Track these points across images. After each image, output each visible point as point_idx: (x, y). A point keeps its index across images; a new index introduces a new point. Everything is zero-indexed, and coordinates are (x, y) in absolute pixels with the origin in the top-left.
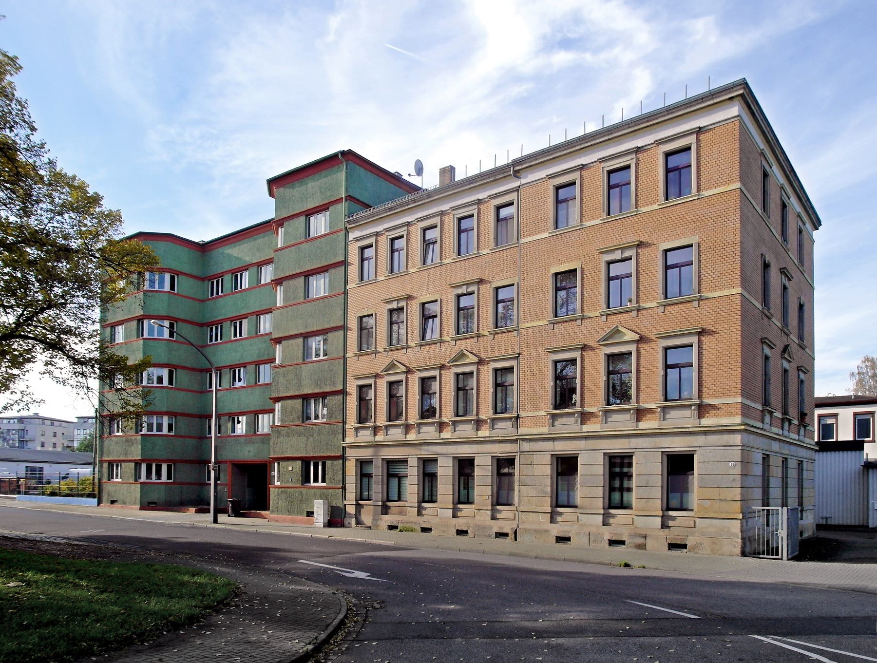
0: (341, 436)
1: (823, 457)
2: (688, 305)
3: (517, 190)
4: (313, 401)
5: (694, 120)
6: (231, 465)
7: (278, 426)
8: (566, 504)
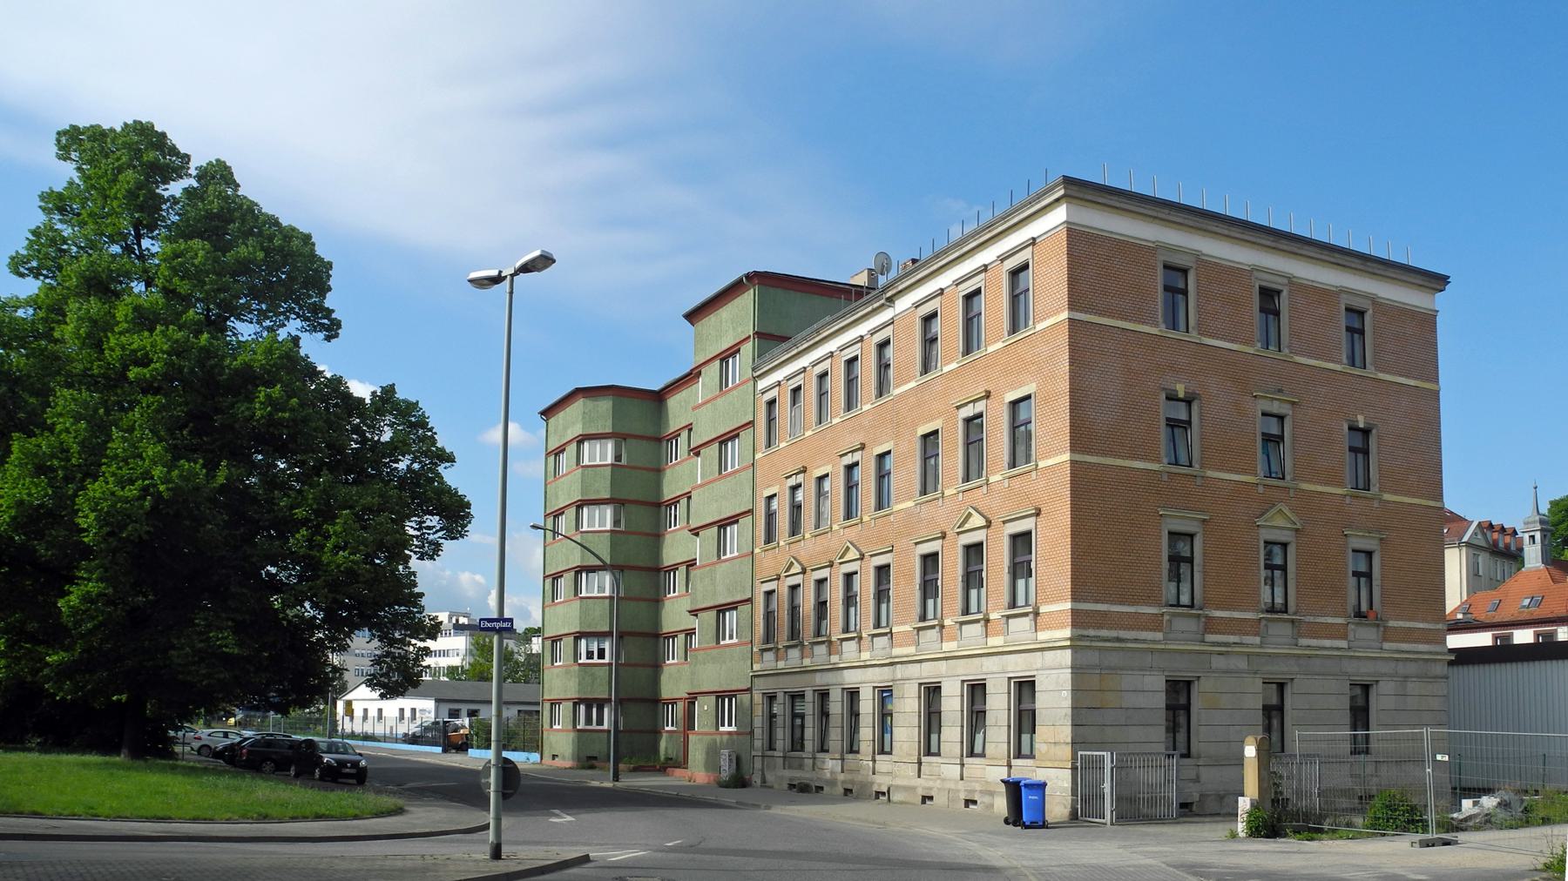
3: (891, 322)
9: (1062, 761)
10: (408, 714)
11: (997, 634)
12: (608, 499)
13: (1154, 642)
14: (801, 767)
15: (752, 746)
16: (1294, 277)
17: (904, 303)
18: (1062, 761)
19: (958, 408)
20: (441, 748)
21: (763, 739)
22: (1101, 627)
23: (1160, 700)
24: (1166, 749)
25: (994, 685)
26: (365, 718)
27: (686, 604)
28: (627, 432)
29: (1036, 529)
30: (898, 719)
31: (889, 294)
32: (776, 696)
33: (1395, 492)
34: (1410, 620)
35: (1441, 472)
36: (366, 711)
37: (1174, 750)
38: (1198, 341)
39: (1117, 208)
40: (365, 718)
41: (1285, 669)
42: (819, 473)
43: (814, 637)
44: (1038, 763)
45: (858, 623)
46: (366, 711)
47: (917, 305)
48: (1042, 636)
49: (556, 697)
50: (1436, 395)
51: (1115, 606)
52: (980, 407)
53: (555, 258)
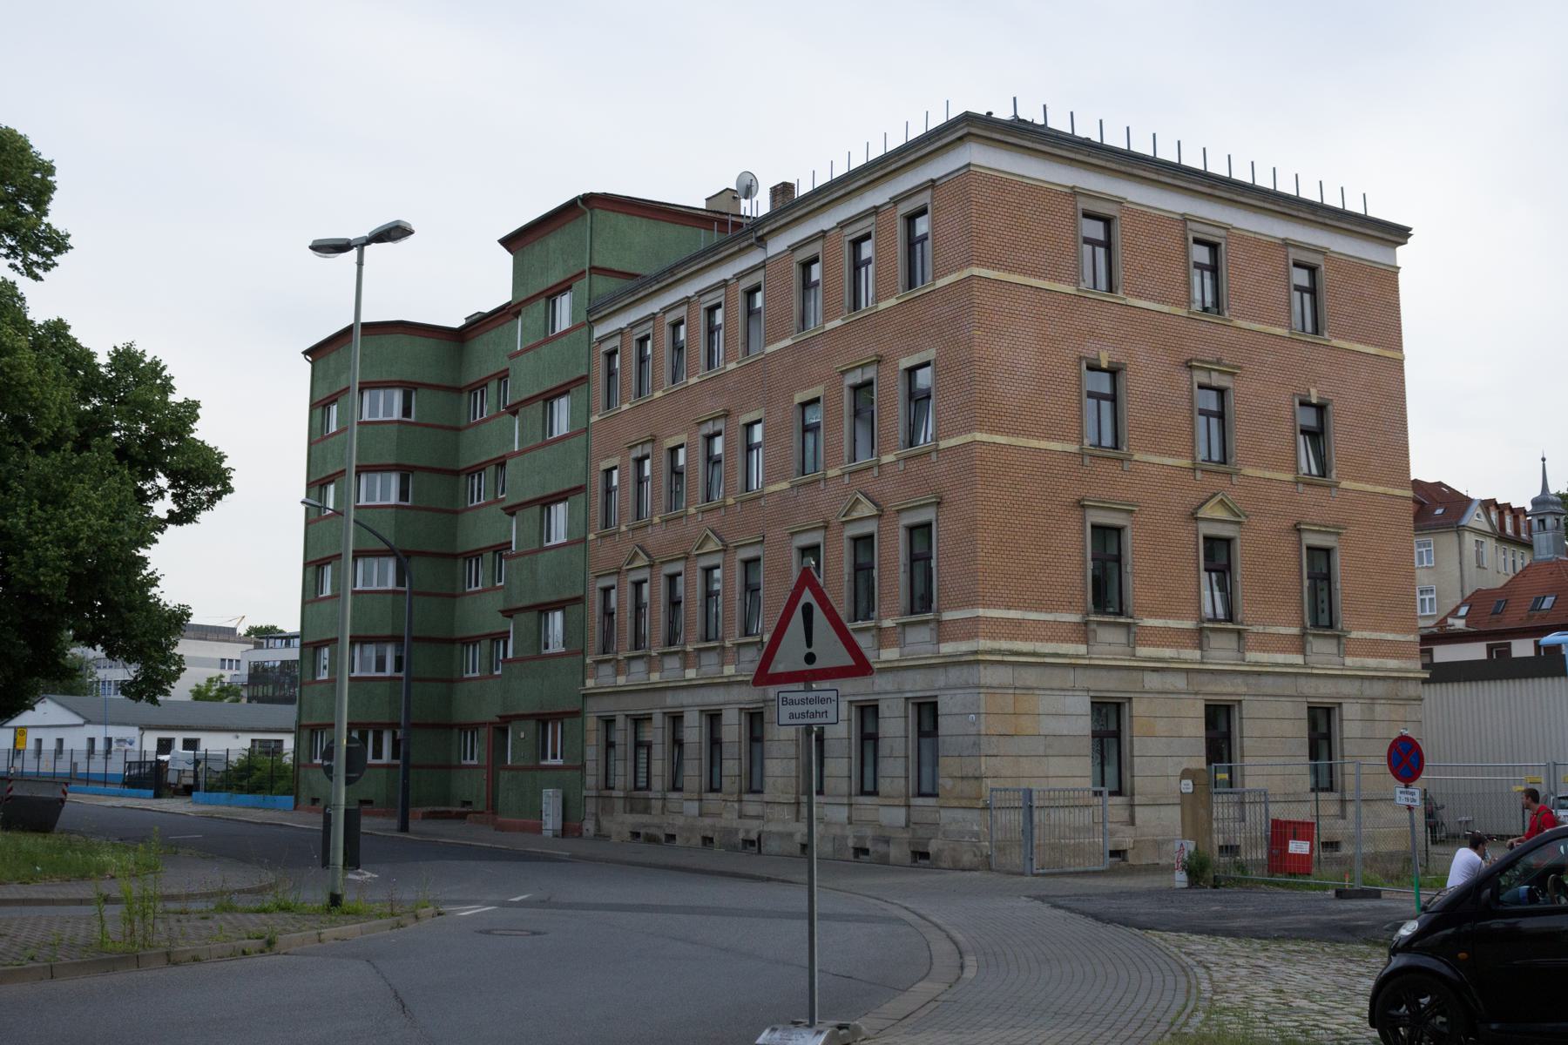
0: (580, 678)
1: (1447, 692)
3: (762, 266)
5: (923, 167)
6: (491, 729)
7: (510, 661)
9: (970, 798)
10: (100, 746)
11: (891, 646)
12: (392, 465)
13: (1077, 657)
14: (647, 810)
15: (583, 783)
16: (1234, 228)
17: (777, 245)
18: (970, 798)
19: (843, 373)
20: (152, 791)
21: (664, 760)
22: (1013, 638)
23: (1084, 725)
24: (1094, 785)
25: (888, 707)
26: (39, 751)
27: (495, 602)
28: (419, 381)
29: (937, 520)
30: (771, 748)
31: (760, 233)
32: (651, 719)
33: (1355, 479)
34: (1375, 630)
35: (1407, 455)
36: (39, 741)
37: (1103, 785)
38: (1123, 302)
39: (1028, 148)
40: (39, 751)
41: (1230, 689)
42: (671, 443)
43: (665, 646)
44: (941, 802)
45: (720, 629)
46: (39, 741)
47: (794, 248)
48: (947, 648)
49: (318, 722)
50: (1399, 364)
51: (1030, 613)
52: (870, 373)
53: (413, 228)
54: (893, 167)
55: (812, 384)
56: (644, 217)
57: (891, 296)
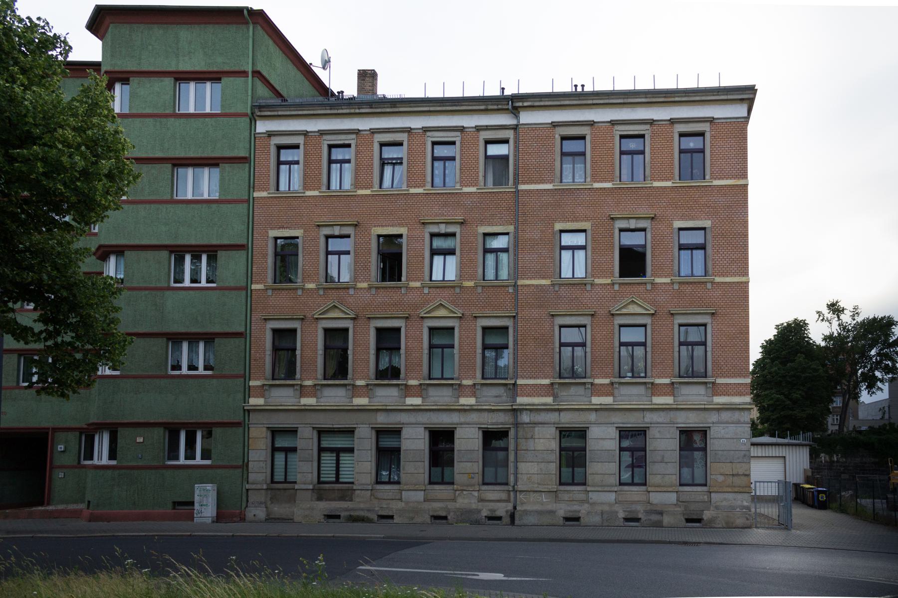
2: (496, 289)
4: (185, 346)
5: (424, 117)
8: (691, 482)
54: (677, 99)
55: (401, 225)
56: (285, 54)
57: (609, 181)
